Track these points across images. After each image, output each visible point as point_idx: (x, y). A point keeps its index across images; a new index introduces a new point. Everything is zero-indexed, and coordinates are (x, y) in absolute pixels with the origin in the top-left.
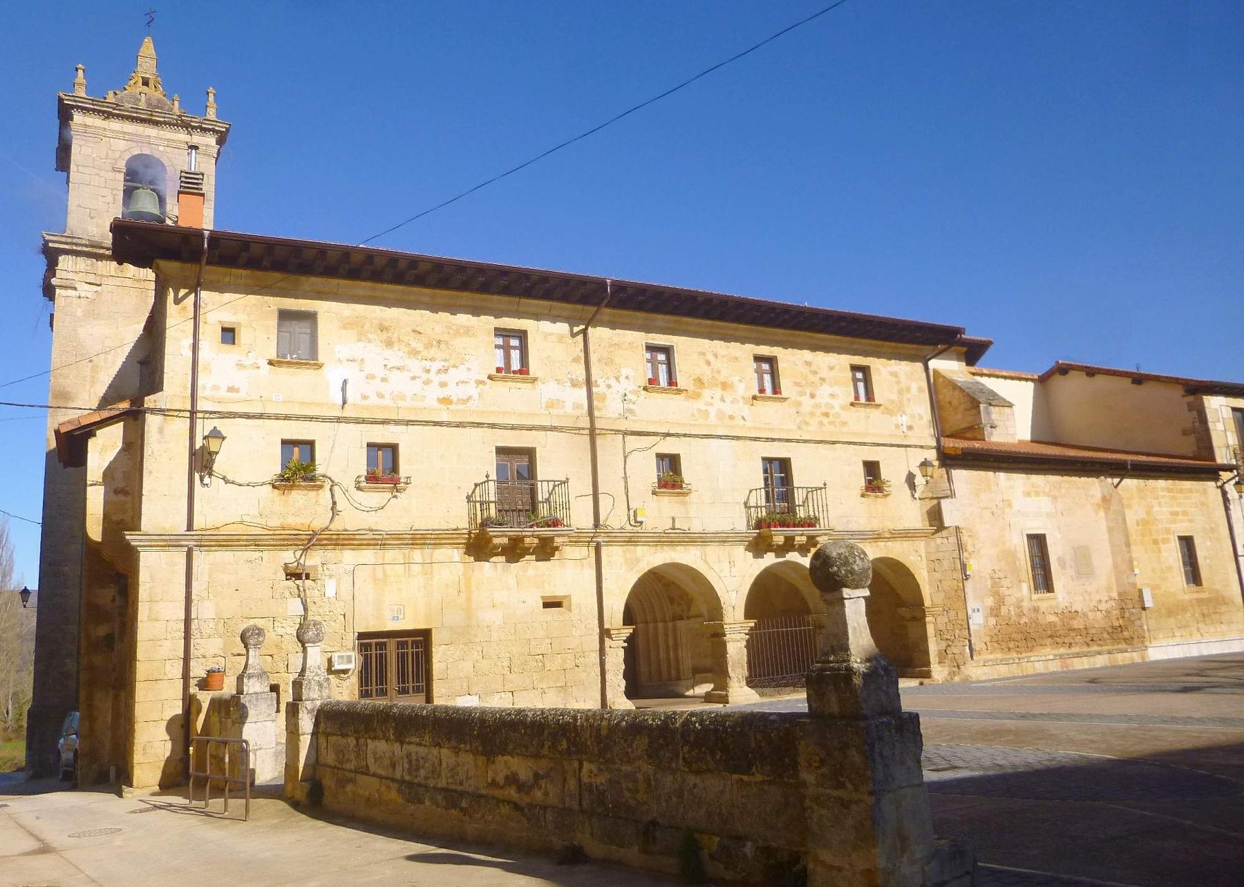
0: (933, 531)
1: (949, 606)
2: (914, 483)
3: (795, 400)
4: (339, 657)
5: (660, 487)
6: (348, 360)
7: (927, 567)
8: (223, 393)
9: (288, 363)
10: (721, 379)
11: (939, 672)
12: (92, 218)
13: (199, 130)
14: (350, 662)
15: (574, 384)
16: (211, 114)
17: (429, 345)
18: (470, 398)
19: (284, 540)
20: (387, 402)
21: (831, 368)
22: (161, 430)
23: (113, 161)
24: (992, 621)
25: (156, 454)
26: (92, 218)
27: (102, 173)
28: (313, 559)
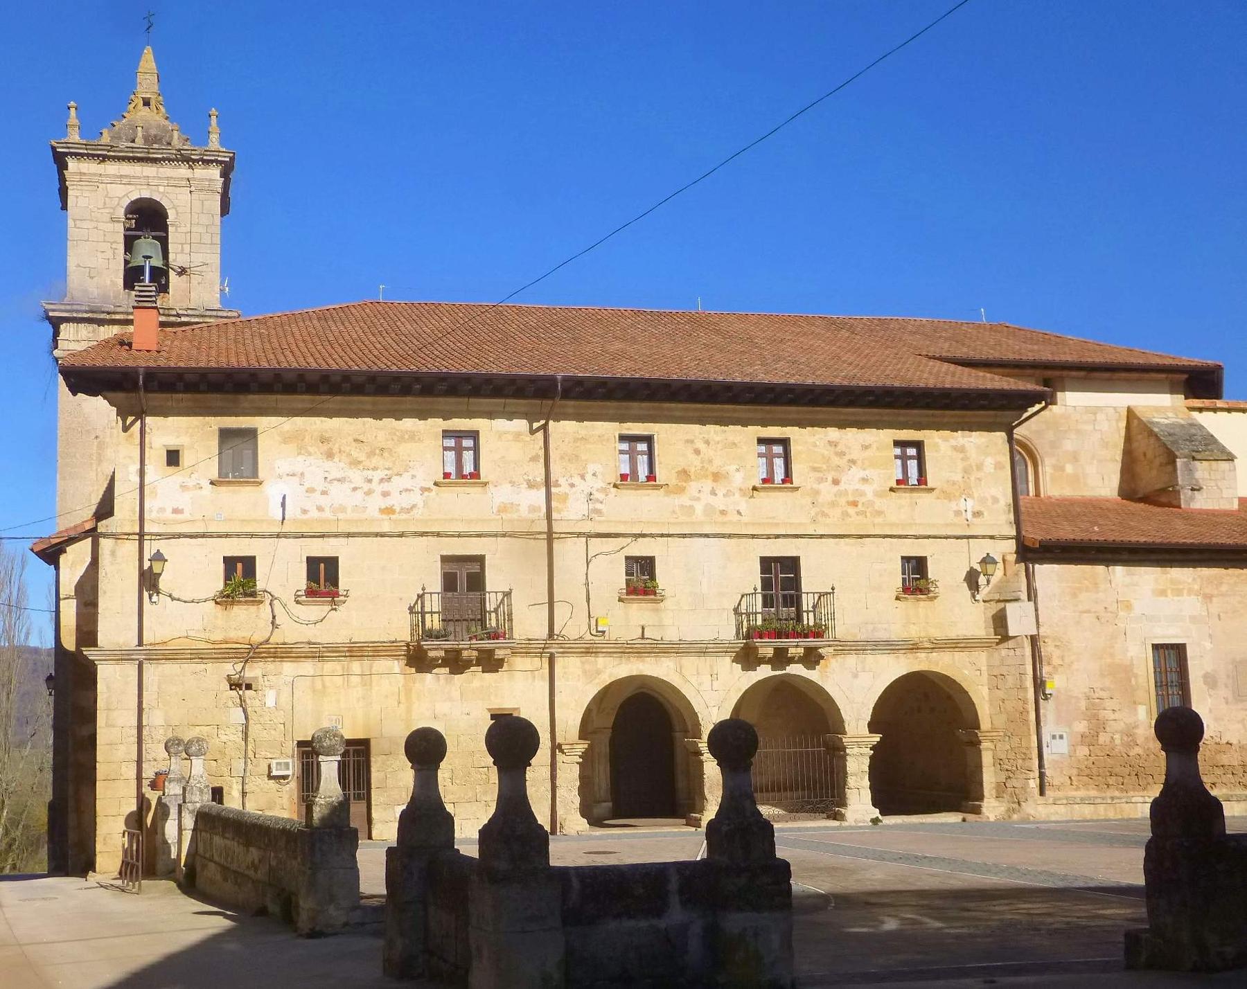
0: (997, 640)
1: (1012, 731)
2: (977, 582)
3: (812, 488)
4: (277, 764)
5: (628, 594)
6: (288, 475)
7: (989, 683)
8: (168, 515)
9: (229, 482)
10: (713, 469)
11: (992, 808)
12: (92, 278)
13: (200, 163)
14: (288, 769)
15: (531, 485)
16: (214, 142)
17: (371, 454)
18: (414, 506)
19: (224, 653)
20: (327, 514)
21: (866, 447)
22: (113, 553)
23: (112, 211)
24: (1083, 751)
25: (109, 576)
26: (92, 278)
27: (101, 226)
28: (253, 671)
